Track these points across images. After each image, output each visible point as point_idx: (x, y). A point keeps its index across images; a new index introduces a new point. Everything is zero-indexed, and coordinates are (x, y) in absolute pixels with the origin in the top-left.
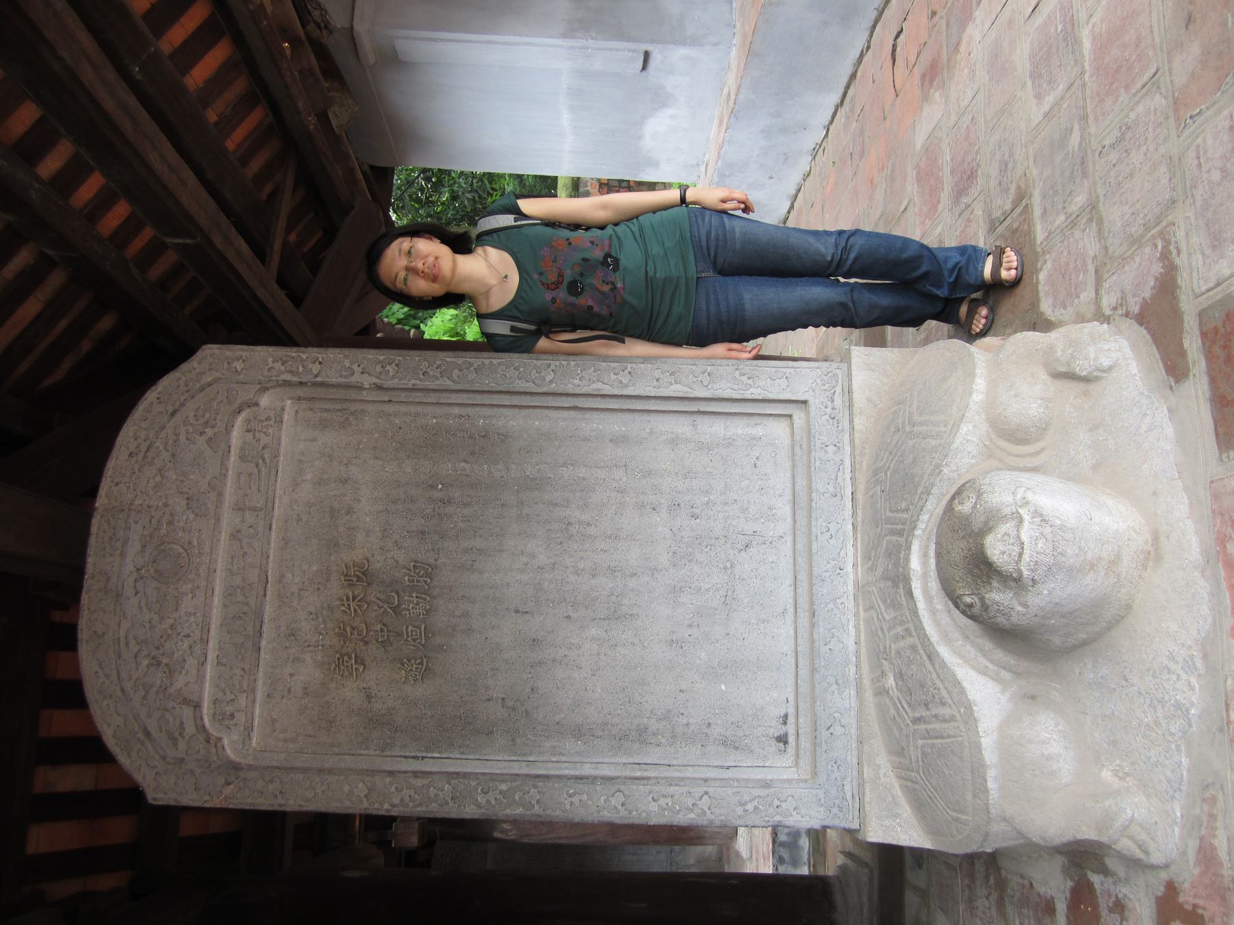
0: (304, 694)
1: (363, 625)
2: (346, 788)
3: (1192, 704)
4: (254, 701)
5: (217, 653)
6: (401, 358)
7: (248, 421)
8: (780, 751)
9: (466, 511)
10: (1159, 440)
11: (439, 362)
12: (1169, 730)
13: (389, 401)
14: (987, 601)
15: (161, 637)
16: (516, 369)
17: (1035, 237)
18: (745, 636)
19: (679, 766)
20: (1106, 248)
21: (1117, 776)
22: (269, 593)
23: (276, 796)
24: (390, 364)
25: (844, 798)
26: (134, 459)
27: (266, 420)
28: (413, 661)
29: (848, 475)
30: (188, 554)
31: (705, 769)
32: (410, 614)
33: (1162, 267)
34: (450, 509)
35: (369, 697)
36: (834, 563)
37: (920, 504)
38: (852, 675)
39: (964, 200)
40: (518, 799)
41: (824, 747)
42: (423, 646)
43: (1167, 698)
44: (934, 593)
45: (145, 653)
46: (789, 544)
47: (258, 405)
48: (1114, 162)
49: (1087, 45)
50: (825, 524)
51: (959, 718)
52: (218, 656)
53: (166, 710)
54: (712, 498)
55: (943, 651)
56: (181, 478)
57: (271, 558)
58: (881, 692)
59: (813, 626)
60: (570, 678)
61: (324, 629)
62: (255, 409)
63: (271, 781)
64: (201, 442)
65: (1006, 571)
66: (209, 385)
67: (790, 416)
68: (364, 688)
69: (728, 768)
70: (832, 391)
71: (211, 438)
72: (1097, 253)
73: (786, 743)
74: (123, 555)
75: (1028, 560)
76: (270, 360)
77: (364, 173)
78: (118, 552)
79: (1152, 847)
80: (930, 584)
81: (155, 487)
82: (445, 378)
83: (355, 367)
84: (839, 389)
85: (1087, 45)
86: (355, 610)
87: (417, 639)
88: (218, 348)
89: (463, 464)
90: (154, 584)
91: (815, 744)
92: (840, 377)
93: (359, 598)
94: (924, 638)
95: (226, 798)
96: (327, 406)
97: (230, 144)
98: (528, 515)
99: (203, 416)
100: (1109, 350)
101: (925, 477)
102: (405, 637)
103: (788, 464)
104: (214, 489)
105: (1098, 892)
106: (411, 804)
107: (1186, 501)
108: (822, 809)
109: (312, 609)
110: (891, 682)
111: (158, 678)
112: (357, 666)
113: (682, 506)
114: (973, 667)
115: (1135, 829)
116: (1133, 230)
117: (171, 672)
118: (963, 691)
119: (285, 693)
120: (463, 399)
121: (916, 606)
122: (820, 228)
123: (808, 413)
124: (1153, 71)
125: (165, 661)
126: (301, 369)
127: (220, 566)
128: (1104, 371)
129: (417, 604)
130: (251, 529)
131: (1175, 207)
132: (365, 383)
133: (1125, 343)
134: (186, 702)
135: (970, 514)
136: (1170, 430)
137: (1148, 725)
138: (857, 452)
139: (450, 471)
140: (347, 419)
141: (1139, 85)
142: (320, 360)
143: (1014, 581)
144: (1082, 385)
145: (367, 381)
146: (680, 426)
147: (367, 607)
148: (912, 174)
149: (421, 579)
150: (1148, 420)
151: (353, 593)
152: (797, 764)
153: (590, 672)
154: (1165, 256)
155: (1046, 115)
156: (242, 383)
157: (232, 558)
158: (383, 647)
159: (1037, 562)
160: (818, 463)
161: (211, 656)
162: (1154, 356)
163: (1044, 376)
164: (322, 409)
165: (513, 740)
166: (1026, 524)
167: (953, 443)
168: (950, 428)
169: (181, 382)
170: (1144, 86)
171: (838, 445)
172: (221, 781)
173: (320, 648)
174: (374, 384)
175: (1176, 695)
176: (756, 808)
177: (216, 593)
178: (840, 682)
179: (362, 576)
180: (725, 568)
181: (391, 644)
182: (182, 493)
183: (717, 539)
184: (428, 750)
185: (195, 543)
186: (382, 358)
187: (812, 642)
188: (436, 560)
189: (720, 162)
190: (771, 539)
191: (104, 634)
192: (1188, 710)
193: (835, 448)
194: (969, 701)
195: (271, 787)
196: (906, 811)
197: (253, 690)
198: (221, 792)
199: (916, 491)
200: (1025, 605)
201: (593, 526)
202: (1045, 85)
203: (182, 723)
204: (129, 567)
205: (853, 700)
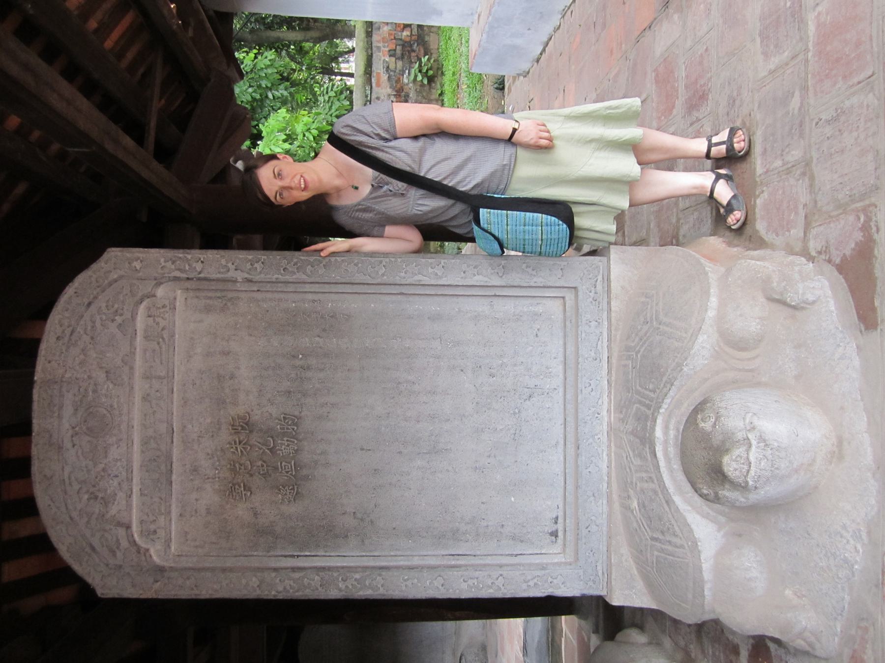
0: (207, 513)
1: (248, 462)
2: (244, 581)
3: (856, 562)
4: (170, 520)
5: (140, 487)
6: (265, 257)
7: (149, 309)
8: (552, 542)
9: (321, 375)
10: (848, 368)
11: (295, 260)
12: (838, 575)
13: (258, 290)
14: (720, 495)
15: (96, 478)
16: (356, 265)
17: (755, 169)
18: (529, 462)
19: (482, 556)
20: (816, 202)
21: (796, 595)
22: (175, 440)
23: (192, 589)
24: (257, 262)
25: (597, 575)
26: (61, 342)
27: (163, 307)
28: (287, 488)
29: (605, 344)
30: (111, 414)
31: (500, 557)
32: (283, 453)
33: (862, 236)
34: (309, 374)
35: (255, 514)
36: (593, 409)
37: (665, 390)
38: (604, 490)
39: (696, 114)
40: (368, 585)
41: (584, 541)
42: (294, 476)
43: (838, 553)
44: (672, 456)
45: (84, 490)
46: (561, 394)
47: (155, 296)
48: (828, 135)
49: (812, 28)
50: (588, 381)
51: (687, 548)
52: (140, 489)
53: (105, 531)
54: (505, 361)
55: (677, 499)
56: (101, 356)
57: (175, 413)
58: (627, 508)
59: (577, 455)
60: (402, 496)
61: (219, 465)
62: (154, 298)
63: (188, 578)
64: (113, 328)
65: (738, 482)
66: (116, 281)
67: (563, 298)
68: (252, 508)
69: (516, 555)
70: (595, 279)
71: (120, 324)
72: (808, 203)
73: (556, 536)
74: (60, 417)
75: (753, 475)
76: (162, 260)
77: (210, 18)
78: (56, 414)
79: (818, 646)
80: (669, 449)
81: (80, 363)
82: (301, 273)
83: (230, 265)
84: (600, 278)
85: (812, 28)
86: (242, 452)
87: (289, 471)
88: (120, 251)
89: (317, 339)
90: (88, 438)
91: (577, 538)
92: (601, 268)
93: (244, 442)
94: (664, 488)
95: (156, 591)
96: (210, 294)
97: (109, 44)
98: (368, 377)
99: (113, 307)
100: (813, 287)
101: (669, 370)
102: (280, 470)
103: (561, 334)
104: (126, 364)
105: (773, 654)
106: (291, 591)
107: (866, 419)
108: (581, 583)
109: (210, 452)
110: (635, 504)
111: (97, 508)
112: (245, 492)
113: (483, 368)
114: (698, 513)
115: (807, 634)
116: (840, 196)
117: (106, 502)
118: (691, 531)
119: (193, 513)
120: (316, 288)
121: (658, 464)
122: (689, 485)
123: (577, 296)
124: (870, 73)
125: (100, 495)
126: (187, 267)
127: (136, 423)
128: (809, 304)
129: (288, 446)
130: (157, 393)
131: (877, 193)
132: (238, 278)
133: (826, 283)
134: (119, 524)
135: (711, 432)
136: (857, 362)
137: (822, 568)
138: (613, 328)
139: (308, 344)
140: (226, 304)
141: (856, 80)
142: (202, 259)
143: (743, 487)
144: (790, 310)
145: (240, 276)
146: (481, 306)
147: (250, 449)
148: (651, 76)
149: (289, 427)
150: (840, 350)
151: (239, 439)
152: (564, 551)
153: (417, 492)
154: (865, 228)
155: (771, 72)
156: (142, 279)
157: (145, 415)
158: (264, 477)
159: (759, 476)
160: (583, 335)
161: (136, 489)
162: (849, 302)
163: (762, 300)
164: (206, 296)
165: (363, 541)
166: (753, 448)
167: (692, 349)
168: (690, 335)
169: (93, 279)
170: (859, 83)
171: (598, 321)
172: (151, 580)
173: (217, 479)
174: (246, 278)
175: (845, 553)
176: (535, 584)
177: (135, 442)
178: (596, 495)
179: (245, 425)
180: (515, 413)
181: (270, 476)
182: (101, 368)
183: (508, 392)
184: (301, 550)
185: (116, 406)
186: (250, 257)
187: (577, 466)
188: (300, 413)
189: (490, 18)
190: (547, 391)
191: (52, 477)
192: (853, 566)
193: (597, 323)
194: (695, 538)
195: (188, 582)
196: (640, 584)
197: (169, 513)
198: (152, 587)
199: (662, 380)
200: (747, 499)
201: (417, 384)
202: (772, 47)
203: (118, 540)
204: (66, 425)
205: (605, 507)
